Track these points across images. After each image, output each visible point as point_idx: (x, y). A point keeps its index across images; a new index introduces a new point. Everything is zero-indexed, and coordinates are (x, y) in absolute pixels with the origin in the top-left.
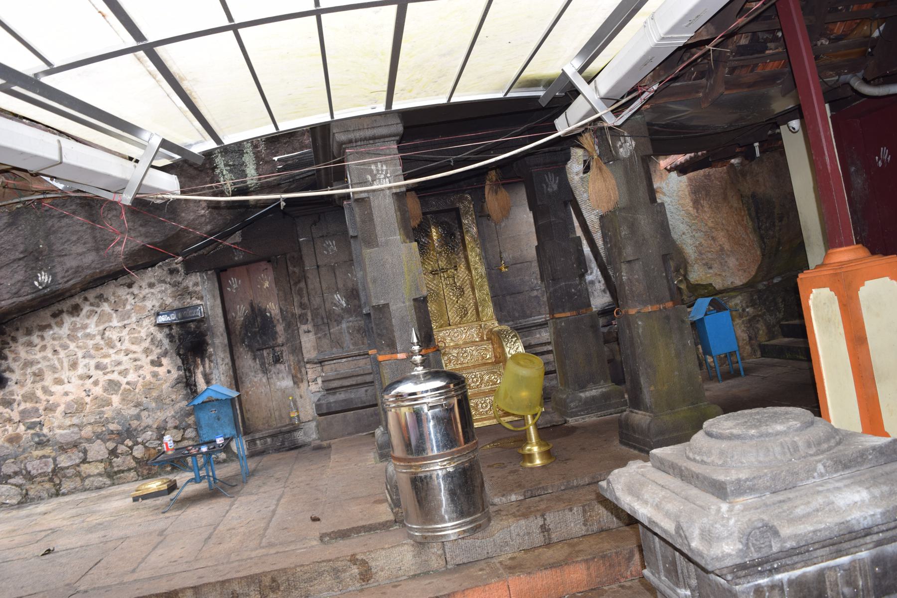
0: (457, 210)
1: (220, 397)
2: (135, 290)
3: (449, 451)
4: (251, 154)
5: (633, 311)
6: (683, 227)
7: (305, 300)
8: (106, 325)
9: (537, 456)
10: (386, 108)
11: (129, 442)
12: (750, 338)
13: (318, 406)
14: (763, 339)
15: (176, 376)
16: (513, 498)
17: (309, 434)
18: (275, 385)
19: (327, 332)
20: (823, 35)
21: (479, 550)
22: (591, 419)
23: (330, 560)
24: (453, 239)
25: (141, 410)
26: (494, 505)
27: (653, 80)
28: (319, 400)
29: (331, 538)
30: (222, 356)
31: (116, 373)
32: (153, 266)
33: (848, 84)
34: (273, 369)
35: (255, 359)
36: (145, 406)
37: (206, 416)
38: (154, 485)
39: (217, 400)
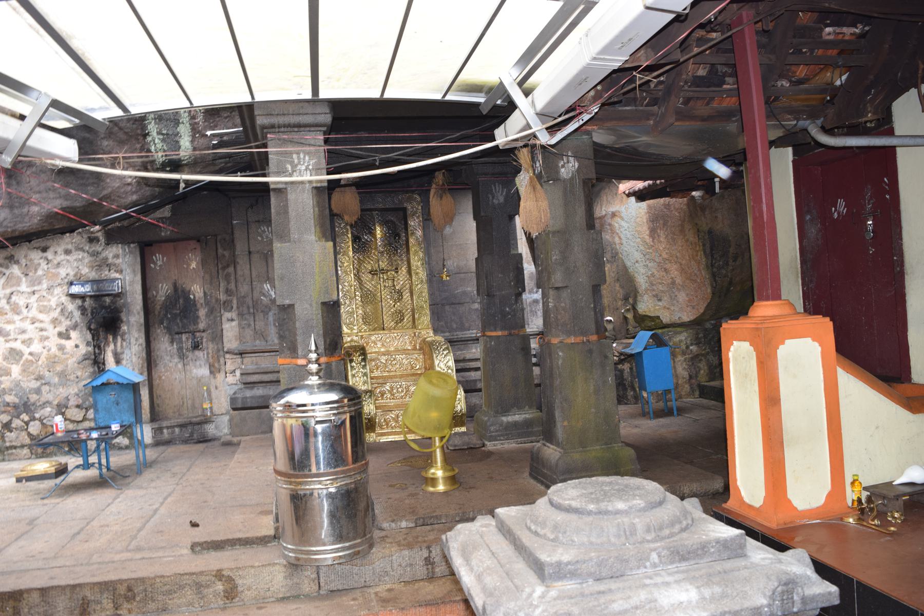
0: (404, 210)
1: (121, 381)
2: (49, 255)
3: (332, 470)
4: (188, 125)
5: (555, 341)
6: (637, 256)
7: (232, 286)
8: (14, 289)
9: (441, 481)
10: (313, 95)
11: (25, 417)
12: (691, 377)
13: (233, 400)
14: (704, 379)
15: (84, 352)
16: (404, 524)
17: (221, 427)
18: (191, 372)
19: (252, 323)
20: (782, 76)
21: (356, 578)
22: (510, 445)
23: (193, 574)
24: (397, 239)
25: (42, 384)
26: (382, 529)
27: (595, 99)
28: (235, 393)
29: (203, 549)
30: (136, 336)
31: (19, 342)
32: (72, 231)
33: (806, 130)
34: (190, 355)
35: (172, 342)
36: (47, 380)
37: (106, 399)
38: (43, 466)
39: (118, 383)
